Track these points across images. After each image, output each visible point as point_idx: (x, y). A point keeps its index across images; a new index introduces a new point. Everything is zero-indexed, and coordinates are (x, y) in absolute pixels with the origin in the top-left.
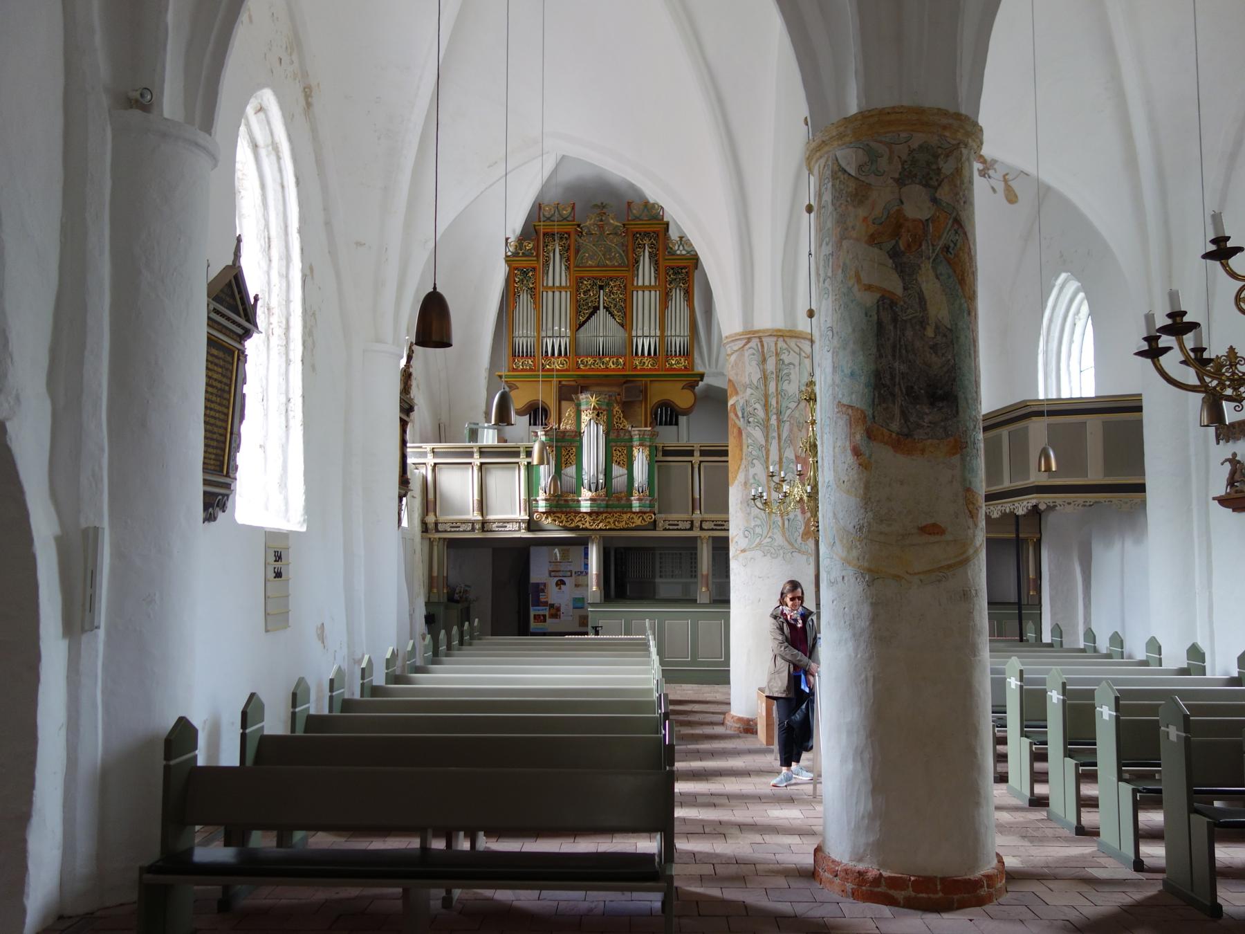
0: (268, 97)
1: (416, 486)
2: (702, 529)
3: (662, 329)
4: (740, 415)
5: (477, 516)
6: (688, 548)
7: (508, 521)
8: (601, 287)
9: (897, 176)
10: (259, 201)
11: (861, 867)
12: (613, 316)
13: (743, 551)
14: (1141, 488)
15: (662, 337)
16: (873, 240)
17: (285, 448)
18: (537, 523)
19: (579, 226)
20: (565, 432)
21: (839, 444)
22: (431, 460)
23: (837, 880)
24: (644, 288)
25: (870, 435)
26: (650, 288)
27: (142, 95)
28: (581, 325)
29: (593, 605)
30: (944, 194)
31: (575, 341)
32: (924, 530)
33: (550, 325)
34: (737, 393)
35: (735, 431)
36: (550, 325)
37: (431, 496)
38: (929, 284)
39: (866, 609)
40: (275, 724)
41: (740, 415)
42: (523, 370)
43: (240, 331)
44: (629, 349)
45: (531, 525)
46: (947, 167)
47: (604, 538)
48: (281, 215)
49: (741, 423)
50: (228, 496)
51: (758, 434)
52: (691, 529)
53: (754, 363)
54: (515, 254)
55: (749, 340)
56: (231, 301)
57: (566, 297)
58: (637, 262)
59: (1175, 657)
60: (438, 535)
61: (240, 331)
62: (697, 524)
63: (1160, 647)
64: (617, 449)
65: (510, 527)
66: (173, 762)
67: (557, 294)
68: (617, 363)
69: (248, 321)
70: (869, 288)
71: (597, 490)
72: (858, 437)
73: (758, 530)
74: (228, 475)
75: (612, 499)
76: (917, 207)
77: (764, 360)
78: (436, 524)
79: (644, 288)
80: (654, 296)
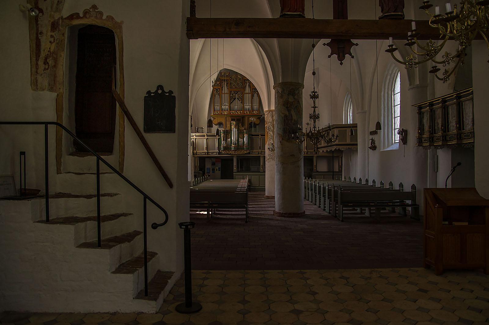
2: (261, 154)
6: (259, 158)
7: (214, 152)
8: (236, 93)
9: (287, 94)
11: (280, 212)
12: (239, 100)
13: (268, 159)
14: (357, 145)
15: (252, 106)
16: (284, 105)
18: (221, 152)
20: (227, 130)
21: (278, 140)
24: (247, 93)
25: (283, 139)
26: (248, 93)
28: (231, 103)
29: (235, 172)
30: (296, 97)
32: (291, 155)
33: (223, 103)
35: (267, 132)
36: (223, 103)
37: (195, 146)
38: (293, 113)
39: (282, 169)
42: (217, 114)
44: (243, 109)
45: (219, 153)
46: (296, 92)
47: (237, 156)
49: (268, 131)
51: (271, 133)
52: (259, 154)
53: (271, 117)
54: (214, 85)
57: (227, 95)
62: (260, 153)
64: (240, 134)
65: (214, 154)
67: (225, 92)
68: (240, 112)
70: (283, 113)
71: (235, 145)
73: (271, 155)
75: (239, 147)
76: (291, 100)
77: (273, 117)
78: (196, 153)
79: (247, 93)
80: (250, 95)
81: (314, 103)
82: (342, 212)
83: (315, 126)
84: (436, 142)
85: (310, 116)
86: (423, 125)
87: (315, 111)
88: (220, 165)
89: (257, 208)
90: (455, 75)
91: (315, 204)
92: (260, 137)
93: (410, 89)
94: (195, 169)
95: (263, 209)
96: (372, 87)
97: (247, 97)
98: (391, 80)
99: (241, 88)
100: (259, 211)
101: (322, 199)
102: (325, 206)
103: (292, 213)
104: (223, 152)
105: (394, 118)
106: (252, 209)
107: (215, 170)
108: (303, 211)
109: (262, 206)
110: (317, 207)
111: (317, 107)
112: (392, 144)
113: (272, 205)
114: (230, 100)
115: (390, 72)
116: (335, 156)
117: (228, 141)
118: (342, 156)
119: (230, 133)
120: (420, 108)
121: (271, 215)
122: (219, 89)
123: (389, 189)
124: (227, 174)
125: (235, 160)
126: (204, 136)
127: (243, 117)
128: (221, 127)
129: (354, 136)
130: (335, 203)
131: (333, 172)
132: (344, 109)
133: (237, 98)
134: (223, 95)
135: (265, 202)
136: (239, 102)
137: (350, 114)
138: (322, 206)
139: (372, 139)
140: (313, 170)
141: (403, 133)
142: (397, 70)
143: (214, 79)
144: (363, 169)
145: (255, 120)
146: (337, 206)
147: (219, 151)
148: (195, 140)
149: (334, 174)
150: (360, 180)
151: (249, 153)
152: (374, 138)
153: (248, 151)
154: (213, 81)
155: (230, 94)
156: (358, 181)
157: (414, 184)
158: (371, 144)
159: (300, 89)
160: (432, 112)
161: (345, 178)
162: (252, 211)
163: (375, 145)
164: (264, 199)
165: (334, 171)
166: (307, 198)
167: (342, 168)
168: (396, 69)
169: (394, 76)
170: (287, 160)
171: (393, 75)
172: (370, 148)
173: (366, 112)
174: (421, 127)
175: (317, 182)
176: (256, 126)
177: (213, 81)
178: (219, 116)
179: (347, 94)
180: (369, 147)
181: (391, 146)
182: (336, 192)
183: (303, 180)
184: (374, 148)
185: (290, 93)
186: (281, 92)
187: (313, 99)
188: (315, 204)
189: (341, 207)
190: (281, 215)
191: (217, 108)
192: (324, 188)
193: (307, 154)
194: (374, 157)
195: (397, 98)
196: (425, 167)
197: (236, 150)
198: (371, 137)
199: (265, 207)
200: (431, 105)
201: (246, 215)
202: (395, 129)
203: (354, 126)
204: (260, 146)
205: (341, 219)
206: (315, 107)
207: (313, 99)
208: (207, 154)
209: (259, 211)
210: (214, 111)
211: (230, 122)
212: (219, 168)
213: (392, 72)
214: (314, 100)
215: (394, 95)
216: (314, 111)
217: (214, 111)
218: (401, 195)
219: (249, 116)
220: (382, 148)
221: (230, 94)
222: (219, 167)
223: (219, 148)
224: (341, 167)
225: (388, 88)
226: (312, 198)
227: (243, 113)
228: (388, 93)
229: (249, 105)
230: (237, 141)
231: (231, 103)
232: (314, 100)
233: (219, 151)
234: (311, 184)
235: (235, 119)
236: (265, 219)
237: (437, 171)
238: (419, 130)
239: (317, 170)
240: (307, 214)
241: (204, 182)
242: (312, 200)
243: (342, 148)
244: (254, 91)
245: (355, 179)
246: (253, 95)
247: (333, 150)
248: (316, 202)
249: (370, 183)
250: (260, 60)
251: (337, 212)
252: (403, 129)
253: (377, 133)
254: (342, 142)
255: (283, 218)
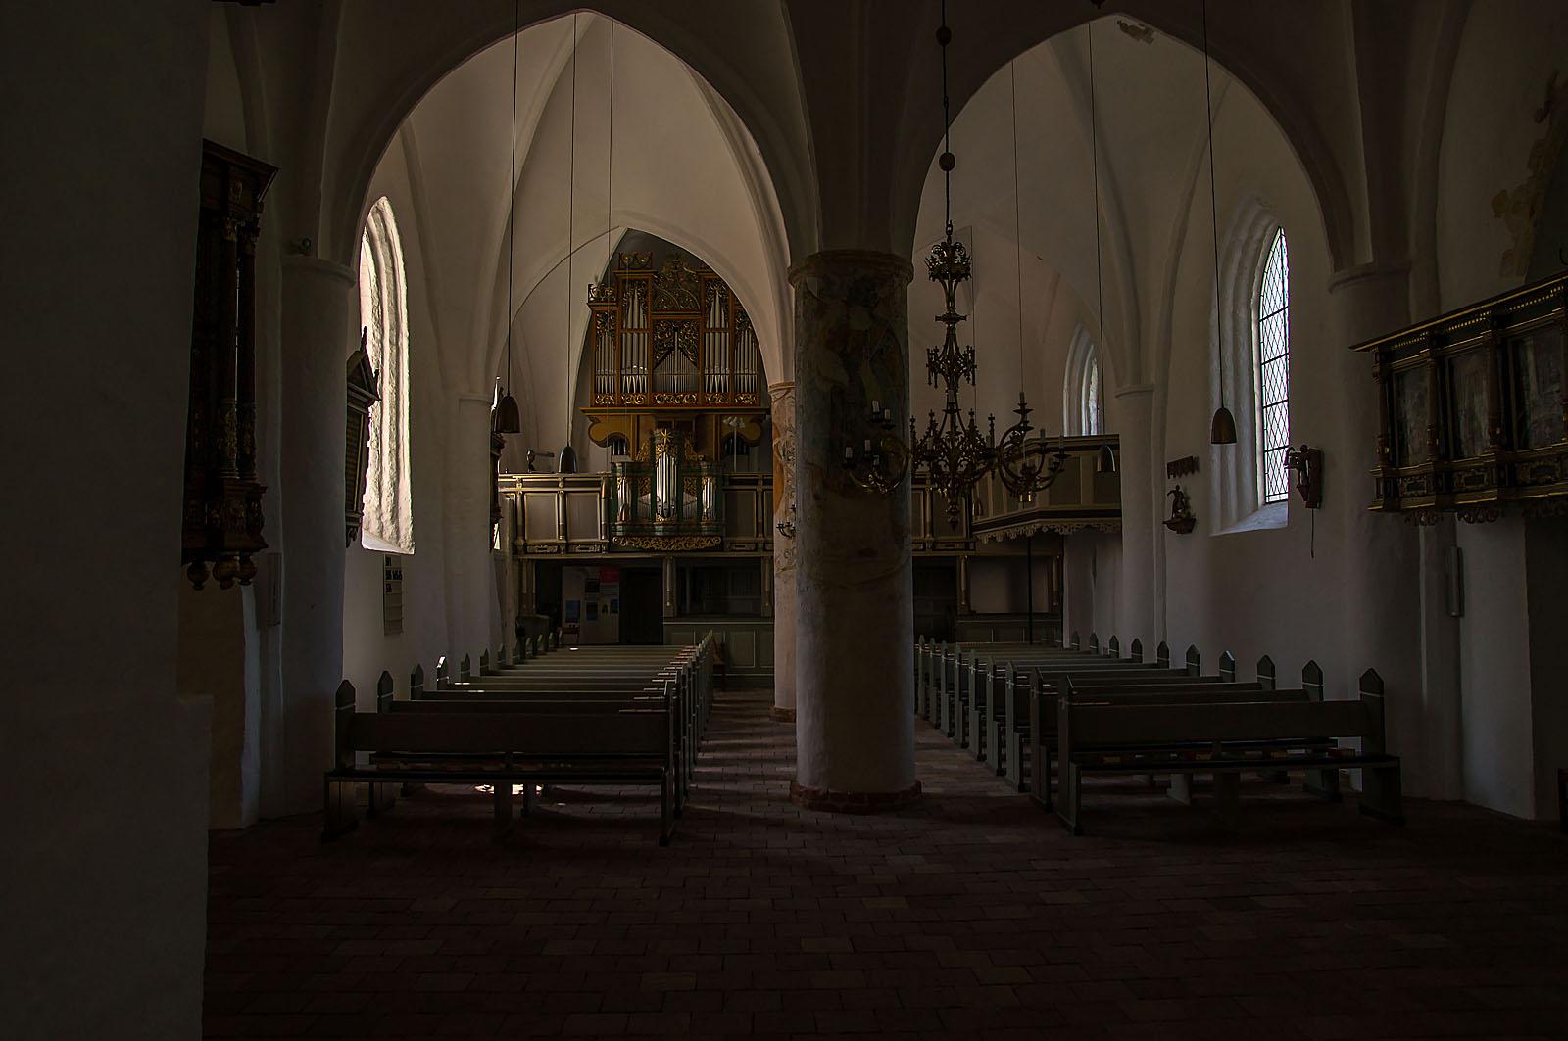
0: (384, 203)
1: (506, 513)
3: (732, 369)
4: (782, 454)
5: (561, 539)
7: (592, 544)
8: (676, 330)
9: (845, 298)
10: (374, 283)
11: (816, 789)
12: (687, 355)
13: (784, 569)
14: (1118, 513)
15: (732, 375)
17: (395, 485)
18: (617, 544)
19: (655, 273)
20: (639, 463)
21: (806, 491)
22: (519, 488)
23: (801, 799)
24: (715, 330)
26: (720, 330)
27: (303, 244)
28: (657, 364)
29: (669, 619)
31: (652, 378)
34: (779, 436)
37: (520, 522)
40: (400, 693)
41: (782, 454)
42: (604, 406)
43: (365, 400)
44: (700, 386)
45: (611, 547)
48: (392, 292)
49: (782, 460)
50: (357, 528)
52: (756, 550)
54: (597, 299)
55: (789, 390)
56: (358, 377)
57: (644, 337)
58: (710, 306)
59: (1150, 657)
60: (527, 557)
61: (365, 400)
62: (761, 546)
63: (1273, 667)
64: (686, 477)
65: (592, 549)
66: (342, 709)
69: (371, 392)
71: (669, 515)
72: (817, 487)
74: (356, 512)
75: (681, 523)
78: (525, 546)
80: (725, 337)
81: (950, 298)
82: (1078, 781)
83: (952, 404)
84: (1467, 491)
85: (930, 360)
86: (1402, 426)
87: (948, 294)
88: (617, 590)
89: (737, 762)
90: (1532, 213)
91: (965, 746)
92: (760, 486)
93: (1337, 284)
94: (520, 607)
95: (756, 769)
96: (1172, 294)
97: (717, 343)
98: (1248, 265)
99: (693, 310)
100: (735, 778)
101: (991, 727)
102: (1003, 766)
103: (867, 793)
104: (624, 541)
105: (1262, 408)
106: (709, 769)
107: (600, 609)
108: (913, 784)
109: (757, 754)
110: (970, 758)
111: (965, 318)
112: (1256, 509)
113: (779, 752)
114: (654, 353)
115: (1243, 236)
116: (1035, 555)
117: (641, 502)
118: (1062, 557)
119: (651, 474)
120: (1386, 354)
121: (782, 799)
122: (615, 313)
123: (1258, 686)
124: (641, 627)
125: (668, 570)
126: (556, 484)
127: (701, 416)
128: (622, 454)
129: (1108, 480)
130: (1043, 748)
131: (1030, 614)
132: (1066, 386)
133: (679, 347)
134: (629, 335)
135: (771, 734)
136: (687, 363)
137: (1087, 404)
138: (991, 753)
139: (1177, 492)
140: (956, 608)
141: (1307, 464)
142: (1267, 228)
143: (596, 279)
144: (1143, 604)
145: (742, 425)
146: (1055, 765)
147: (610, 539)
148: (522, 498)
149: (1033, 624)
150: (1136, 646)
151: (721, 548)
152: (1185, 489)
153: (716, 541)
154: (590, 286)
155: (654, 331)
156: (1126, 653)
157: (1266, 656)
158: (1175, 511)
159: (896, 279)
160: (1444, 369)
161: (1075, 637)
162: (711, 778)
163: (1189, 514)
164: (767, 720)
165: (1034, 611)
166: (933, 719)
167: (1061, 600)
168: (1264, 223)
169: (1258, 250)
170: (846, 566)
171: (1253, 246)
172: (1171, 525)
173: (1152, 391)
174: (1393, 435)
175: (974, 659)
176: (747, 449)
177: (590, 286)
178: (613, 411)
179: (1077, 331)
180: (1164, 523)
181: (1255, 518)
182: (1048, 706)
183: (911, 649)
184: (1183, 522)
185: (852, 294)
186: (820, 292)
187: (946, 282)
188: (965, 746)
189: (1073, 777)
190: (818, 802)
191: (604, 381)
192: (999, 686)
193: (934, 549)
194: (1184, 559)
195: (1274, 336)
196: (1415, 602)
197: (670, 537)
198: (1171, 483)
199: (762, 761)
200: (1438, 338)
201: (663, 799)
202: (1264, 452)
203: (1105, 447)
204: (760, 521)
205: (1074, 825)
206: (951, 318)
207: (946, 282)
208: (567, 551)
209: (735, 778)
210: (596, 391)
211: (651, 432)
212: (613, 603)
213: (1250, 237)
214: (950, 285)
215: (1259, 321)
216: (951, 336)
217: (596, 391)
218: (1307, 714)
219: (722, 413)
220: (1217, 522)
221: (654, 331)
222: (615, 598)
223: (609, 529)
224: (1056, 596)
225: (1235, 300)
226: (950, 719)
227: (699, 403)
228: (1234, 314)
229: (718, 372)
230: (677, 502)
231: (655, 365)
232: (950, 285)
233: (610, 539)
234: (949, 666)
235: (671, 422)
236: (753, 821)
237: (1461, 613)
238: (1384, 444)
239: (972, 609)
240: (928, 795)
241: (541, 659)
242: (951, 725)
243: (1065, 527)
244: (739, 322)
245: (1114, 643)
246: (736, 336)
247: (1029, 534)
248: (966, 734)
249: (1178, 662)
250: (753, 191)
251: (1052, 782)
252: (1304, 448)
253: (1198, 469)
254: (1071, 498)
255: (827, 817)
